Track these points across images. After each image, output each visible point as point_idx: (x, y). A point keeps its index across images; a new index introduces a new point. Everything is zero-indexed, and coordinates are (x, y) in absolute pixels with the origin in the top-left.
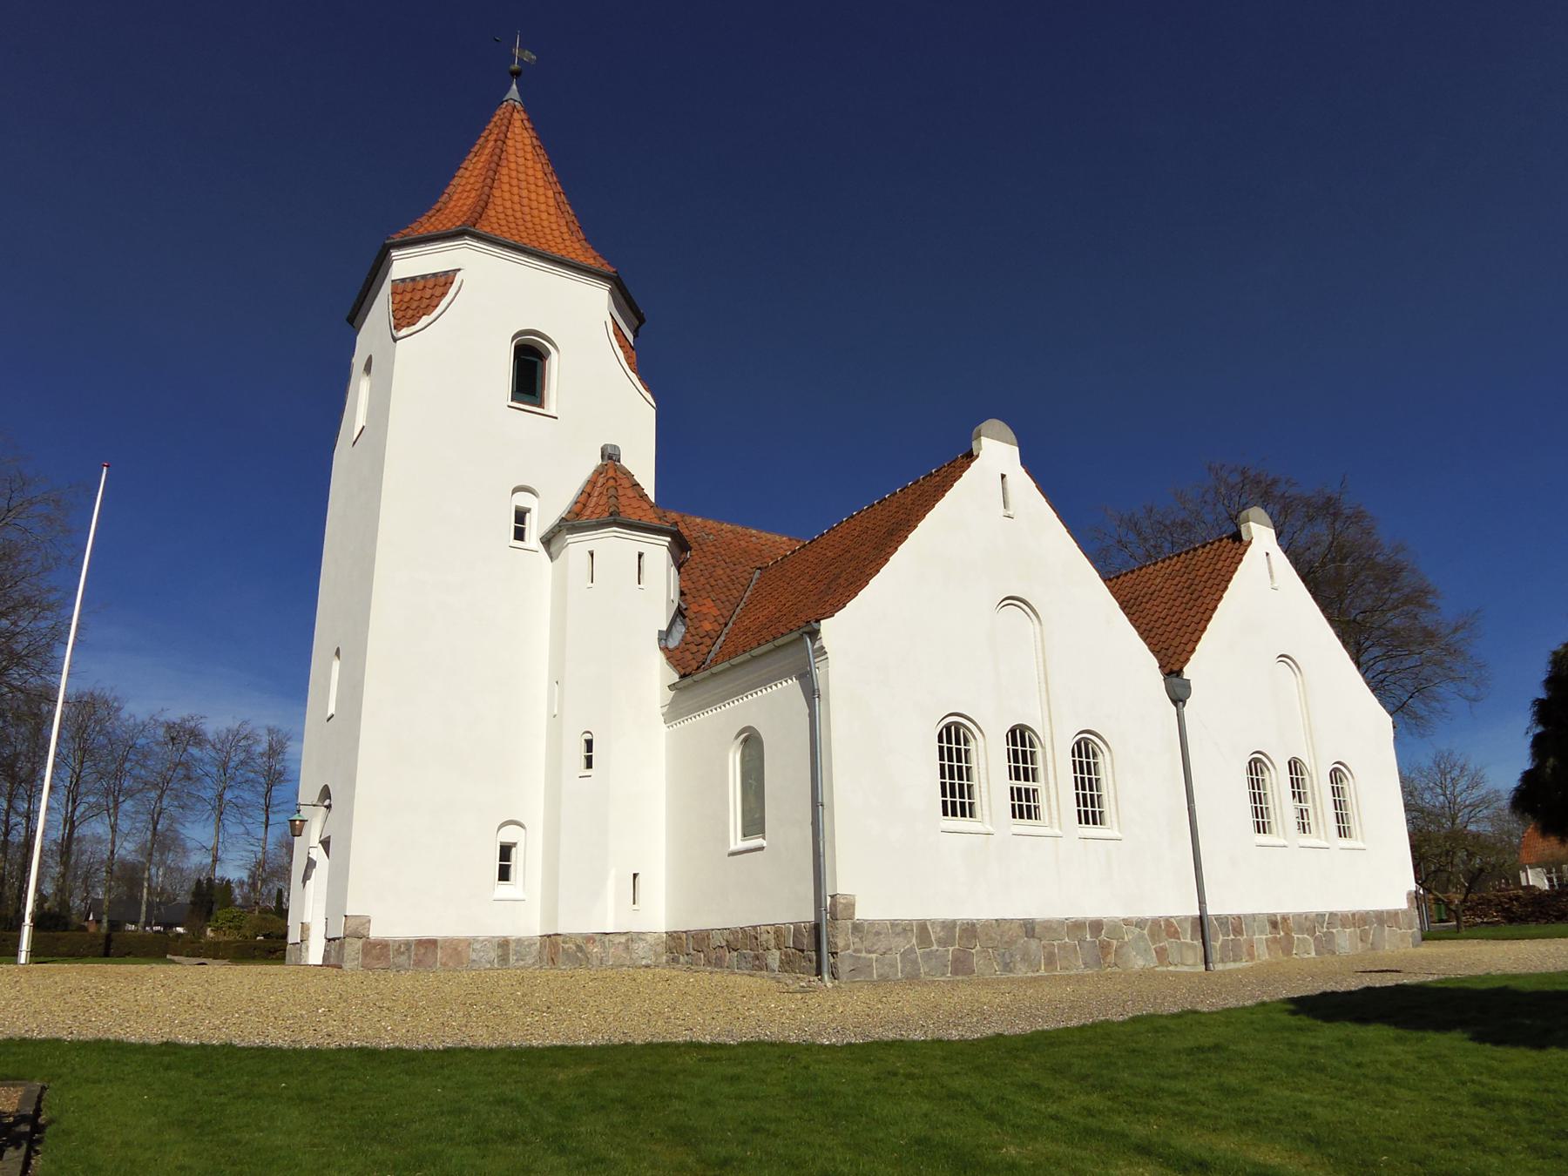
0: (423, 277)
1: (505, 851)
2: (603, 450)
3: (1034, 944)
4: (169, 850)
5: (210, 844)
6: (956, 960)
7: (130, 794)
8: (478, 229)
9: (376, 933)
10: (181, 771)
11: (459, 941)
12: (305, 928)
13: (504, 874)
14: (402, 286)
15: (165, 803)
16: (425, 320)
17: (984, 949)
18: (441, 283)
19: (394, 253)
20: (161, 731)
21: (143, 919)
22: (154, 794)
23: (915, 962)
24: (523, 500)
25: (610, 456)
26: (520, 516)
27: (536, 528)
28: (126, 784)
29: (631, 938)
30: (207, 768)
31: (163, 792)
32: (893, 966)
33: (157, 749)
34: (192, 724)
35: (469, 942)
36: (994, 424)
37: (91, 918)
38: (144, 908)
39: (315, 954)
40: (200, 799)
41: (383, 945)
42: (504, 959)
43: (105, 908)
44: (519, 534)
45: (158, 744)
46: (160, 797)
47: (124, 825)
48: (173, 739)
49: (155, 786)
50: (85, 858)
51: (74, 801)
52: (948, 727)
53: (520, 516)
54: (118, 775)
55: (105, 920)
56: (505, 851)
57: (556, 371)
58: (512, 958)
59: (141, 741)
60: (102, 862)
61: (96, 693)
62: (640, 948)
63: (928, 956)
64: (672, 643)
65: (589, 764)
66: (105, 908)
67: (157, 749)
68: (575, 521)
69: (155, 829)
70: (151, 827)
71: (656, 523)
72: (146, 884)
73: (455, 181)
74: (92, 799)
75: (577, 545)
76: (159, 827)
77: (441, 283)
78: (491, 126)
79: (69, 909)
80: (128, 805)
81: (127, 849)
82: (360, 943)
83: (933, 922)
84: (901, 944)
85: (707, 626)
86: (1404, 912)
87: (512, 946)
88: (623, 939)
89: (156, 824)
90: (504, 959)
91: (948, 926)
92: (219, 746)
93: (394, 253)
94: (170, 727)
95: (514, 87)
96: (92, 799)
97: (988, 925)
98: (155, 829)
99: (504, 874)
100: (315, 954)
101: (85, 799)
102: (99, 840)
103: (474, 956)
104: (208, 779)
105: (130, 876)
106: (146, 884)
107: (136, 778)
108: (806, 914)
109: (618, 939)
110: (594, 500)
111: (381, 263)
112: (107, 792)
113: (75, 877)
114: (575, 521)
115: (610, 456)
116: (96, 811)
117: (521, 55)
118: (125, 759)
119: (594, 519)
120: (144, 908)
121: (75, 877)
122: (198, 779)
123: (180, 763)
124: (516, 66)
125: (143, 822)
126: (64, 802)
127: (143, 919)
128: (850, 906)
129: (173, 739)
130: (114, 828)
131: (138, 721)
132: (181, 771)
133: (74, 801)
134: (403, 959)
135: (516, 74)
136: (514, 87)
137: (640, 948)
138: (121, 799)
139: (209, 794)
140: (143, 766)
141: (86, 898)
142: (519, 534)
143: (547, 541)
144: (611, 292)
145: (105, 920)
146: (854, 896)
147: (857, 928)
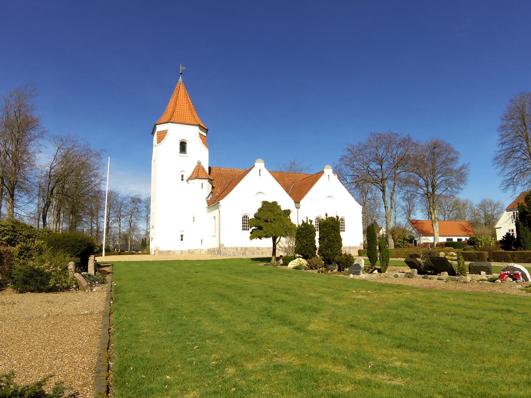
0: (162, 131)
1: (182, 236)
3: (259, 251)
4: (135, 231)
5: (146, 229)
6: (243, 253)
7: (123, 216)
8: (171, 121)
9: (160, 250)
10: (136, 210)
12: (152, 249)
13: (182, 240)
14: (159, 133)
16: (162, 141)
17: (249, 251)
18: (165, 132)
19: (157, 126)
20: (130, 199)
21: (129, 249)
22: (129, 216)
23: (235, 253)
24: (182, 173)
25: (199, 163)
26: (182, 176)
27: (185, 178)
28: (122, 214)
29: (201, 250)
30: (143, 208)
31: (132, 216)
32: (231, 254)
33: (129, 204)
34: (138, 197)
36: (260, 160)
37: (116, 250)
38: (129, 247)
39: (153, 254)
40: (142, 217)
41: (162, 252)
42: (182, 253)
43: (119, 247)
44: (182, 180)
45: (129, 203)
46: (131, 217)
47: (122, 225)
48: (133, 201)
51: (109, 219)
52: (245, 216)
53: (182, 176)
54: (120, 211)
55: (119, 250)
56: (182, 236)
57: (188, 147)
58: (183, 253)
59: (125, 202)
60: (117, 234)
61: (112, 190)
62: (203, 252)
63: (237, 253)
64: (208, 200)
66: (119, 247)
67: (129, 204)
68: (190, 178)
69: (130, 226)
70: (129, 225)
71: (205, 177)
72: (129, 240)
73: (168, 106)
74: (113, 218)
75: (191, 182)
76: (131, 225)
77: (165, 132)
78: (175, 89)
79: (109, 248)
80: (123, 220)
81: (124, 230)
83: (239, 247)
84: (233, 250)
85: (217, 195)
87: (183, 252)
88: (200, 250)
90: (182, 253)
91: (242, 248)
92: (146, 202)
93: (157, 126)
94: (132, 198)
95: (181, 77)
96: (113, 218)
97: (249, 248)
98: (130, 226)
99: (182, 240)
100: (153, 254)
102: (116, 228)
103: (176, 253)
104: (143, 211)
106: (129, 240)
107: (124, 212)
108: (217, 246)
110: (195, 173)
111: (155, 128)
112: (117, 216)
113: (110, 238)
114: (190, 178)
115: (199, 163)
116: (115, 221)
117: (182, 68)
118: (121, 207)
119: (193, 178)
120: (129, 247)
121: (110, 238)
122: (141, 212)
123: (135, 208)
124: (181, 72)
127: (129, 249)
128: (223, 245)
129: (133, 201)
130: (120, 226)
131: (124, 197)
132: (136, 210)
133: (109, 219)
134: (165, 254)
135: (181, 74)
136: (181, 77)
137: (203, 252)
138: (121, 218)
139: (144, 215)
140: (126, 209)
141: (114, 244)
142: (182, 180)
143: (187, 181)
144: (199, 128)
145: (119, 250)
147: (224, 248)
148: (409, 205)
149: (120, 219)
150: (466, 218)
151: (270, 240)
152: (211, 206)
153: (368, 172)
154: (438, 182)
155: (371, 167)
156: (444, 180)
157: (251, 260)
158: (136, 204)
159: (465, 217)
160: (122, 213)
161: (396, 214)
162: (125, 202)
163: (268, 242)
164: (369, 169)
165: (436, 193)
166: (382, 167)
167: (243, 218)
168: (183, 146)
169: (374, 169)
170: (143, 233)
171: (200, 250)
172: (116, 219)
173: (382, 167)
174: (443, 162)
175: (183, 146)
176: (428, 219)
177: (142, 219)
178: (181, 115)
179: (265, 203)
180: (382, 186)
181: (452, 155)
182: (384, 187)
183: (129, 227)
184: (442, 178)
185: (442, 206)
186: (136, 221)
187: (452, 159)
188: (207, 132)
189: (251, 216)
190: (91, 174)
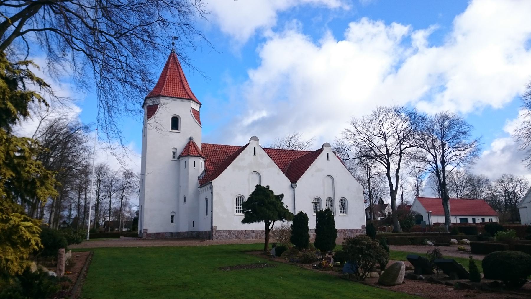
1: (172, 217)
2: (190, 138)
9: (149, 232)
11: (163, 233)
15: (124, 194)
22: (121, 192)
25: (191, 139)
35: (166, 233)
41: (150, 234)
46: (123, 192)
47: (113, 200)
49: (121, 189)
50: (103, 208)
52: (238, 197)
59: (116, 176)
65: (185, 202)
74: (103, 194)
76: (123, 201)
80: (114, 195)
82: (146, 234)
86: (360, 229)
88: (191, 233)
89: (122, 200)
101: (101, 194)
103: (166, 236)
105: (118, 213)
109: (190, 233)
115: (191, 139)
125: (118, 199)
126: (95, 195)
132: (128, 185)
140: (117, 183)
143: (179, 158)
146: (147, 230)
147: (217, 231)
148: (417, 181)
149: (111, 195)
150: (482, 194)
151: (263, 223)
152: (203, 186)
153: (372, 148)
154: (449, 156)
155: (375, 142)
156: (455, 155)
157: (390, 78)
158: (129, 179)
159: (481, 194)
160: (113, 188)
161: (403, 190)
162: (116, 176)
163: (260, 226)
164: (372, 145)
165: (446, 169)
166: (386, 141)
167: (236, 199)
168: (175, 123)
169: (378, 145)
170: (135, 209)
171: (191, 233)
172: (106, 194)
173: (386, 141)
174: (454, 136)
175: (175, 123)
176: (439, 195)
177: (135, 194)
178: (173, 86)
179: (258, 187)
180: (387, 163)
181: (464, 129)
182: (388, 164)
183: (120, 203)
184: (454, 153)
185: (454, 182)
186: (128, 197)
187: (464, 133)
188: (200, 107)
189: (247, 196)
190: (80, 146)
